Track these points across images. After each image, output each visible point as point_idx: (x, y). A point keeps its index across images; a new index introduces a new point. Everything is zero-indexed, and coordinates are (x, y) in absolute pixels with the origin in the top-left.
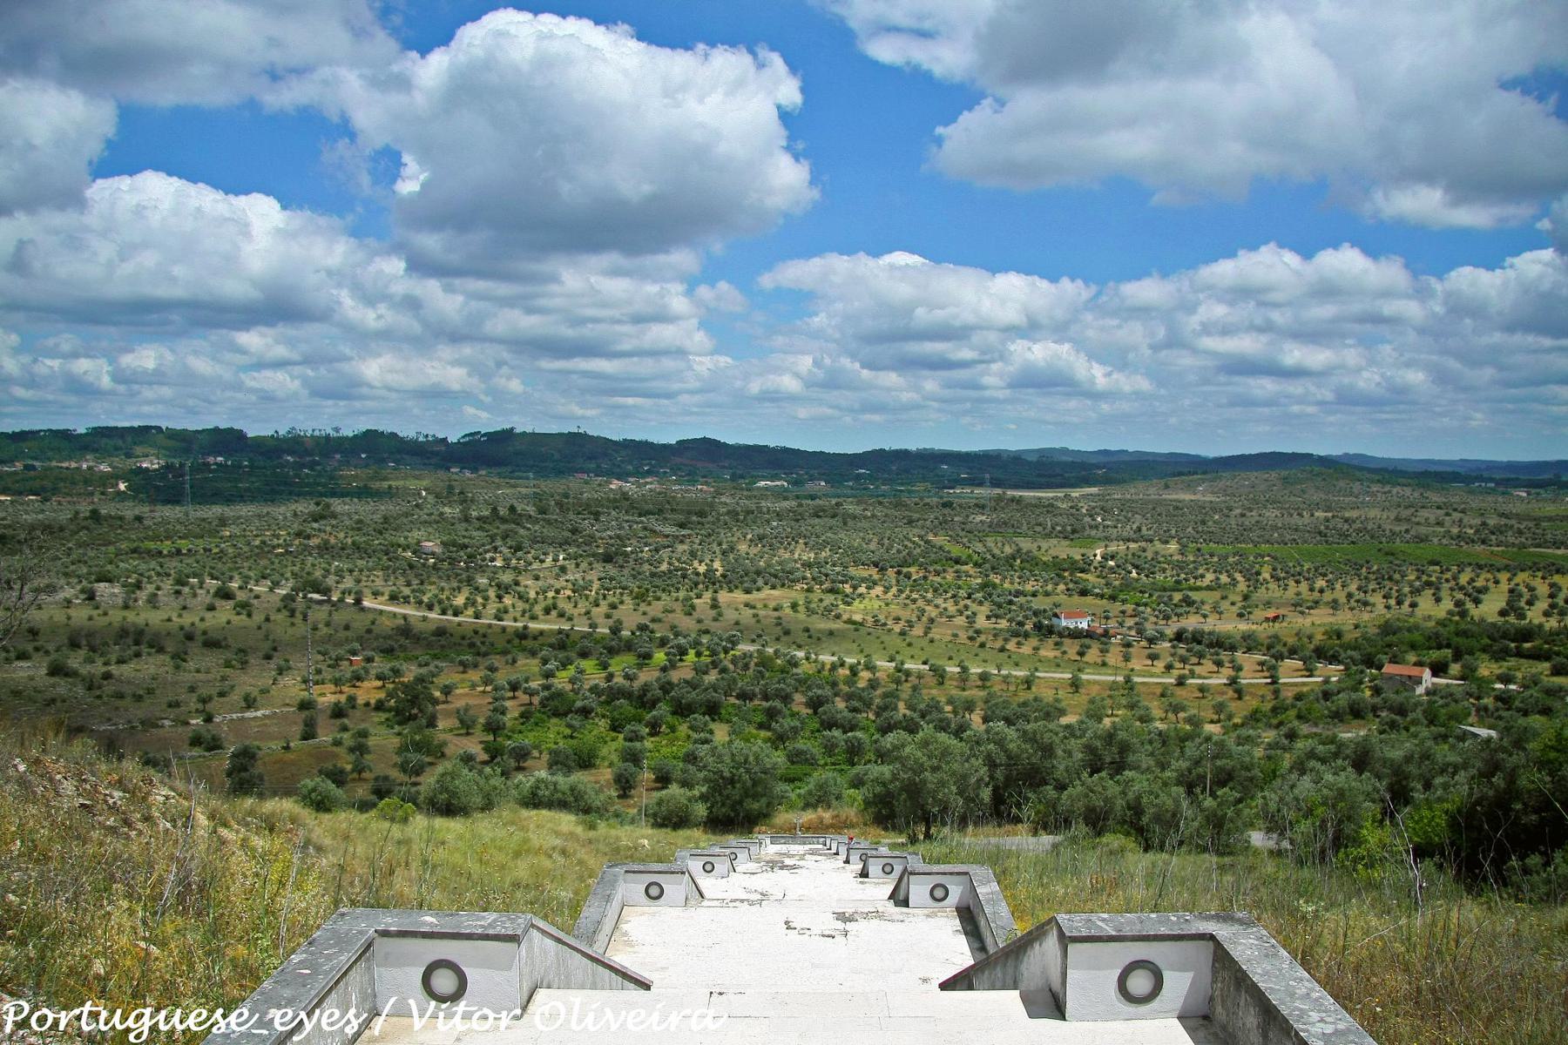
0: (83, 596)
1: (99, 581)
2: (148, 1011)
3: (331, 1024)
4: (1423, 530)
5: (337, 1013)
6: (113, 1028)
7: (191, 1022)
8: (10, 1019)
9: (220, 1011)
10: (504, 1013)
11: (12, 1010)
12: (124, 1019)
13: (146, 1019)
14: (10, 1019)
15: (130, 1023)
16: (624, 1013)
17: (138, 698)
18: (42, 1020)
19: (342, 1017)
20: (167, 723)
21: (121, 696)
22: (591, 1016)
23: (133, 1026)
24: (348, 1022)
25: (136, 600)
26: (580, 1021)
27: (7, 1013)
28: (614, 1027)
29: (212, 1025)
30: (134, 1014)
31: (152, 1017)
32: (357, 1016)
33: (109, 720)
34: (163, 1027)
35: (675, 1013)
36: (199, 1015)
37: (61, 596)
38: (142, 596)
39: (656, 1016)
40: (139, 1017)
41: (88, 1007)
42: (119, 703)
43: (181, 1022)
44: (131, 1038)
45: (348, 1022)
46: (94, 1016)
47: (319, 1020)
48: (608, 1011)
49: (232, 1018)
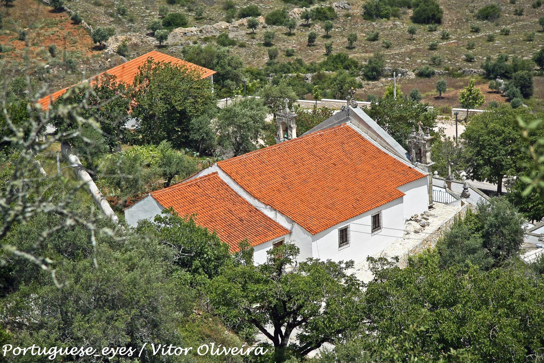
2: (56, 348)
5: (77, 349)
6: (216, 354)
11: (6, 348)
15: (49, 352)
18: (17, 351)
19: (78, 350)
23: (50, 353)
24: (81, 352)
26: (214, 351)
28: (226, 354)
30: (50, 349)
31: (57, 350)
34: (61, 354)
36: (235, 349)
38: (22, 61)
40: (53, 350)
41: (34, 347)
43: (68, 352)
44: (50, 358)
45: (81, 352)
47: (230, 351)
48: (224, 348)
49: (87, 351)
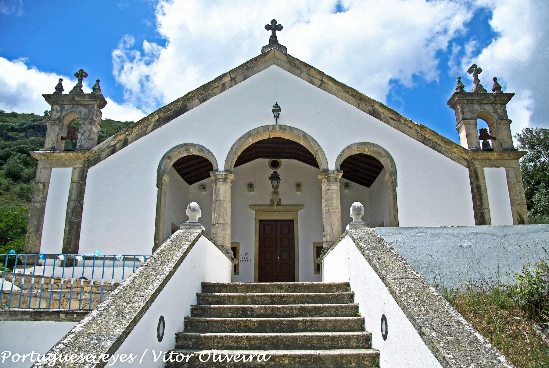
10: (24, 355)
11: (5, 354)
14: (4, 358)
18: (16, 358)
24: (80, 359)
32: (133, 357)
41: (33, 353)
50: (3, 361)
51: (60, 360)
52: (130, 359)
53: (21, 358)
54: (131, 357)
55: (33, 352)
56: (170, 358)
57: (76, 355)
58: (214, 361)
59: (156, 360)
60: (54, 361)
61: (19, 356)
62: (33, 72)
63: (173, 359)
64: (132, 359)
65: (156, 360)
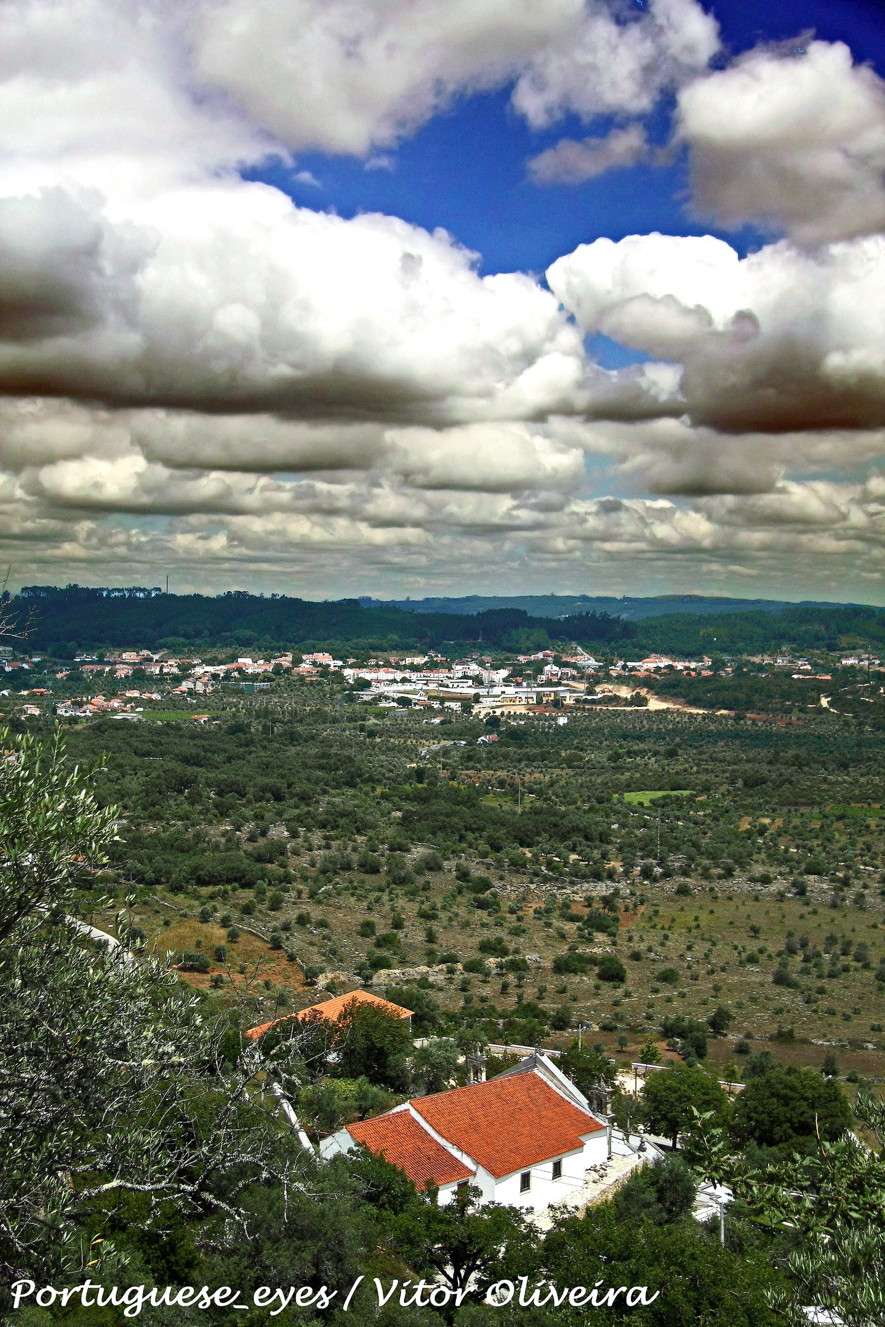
0: (794, 890)
1: (809, 872)
3: (579, 1300)
4: (351, 725)
7: (179, 1298)
8: (18, 1296)
9: (206, 1289)
10: (66, 1291)
11: (20, 1288)
12: (119, 1296)
13: (139, 1296)
14: (18, 1296)
15: (125, 1299)
16: (566, 1290)
17: (847, 1018)
18: (46, 1296)
20: (870, 1046)
21: (832, 1012)
22: (537, 1293)
23: (127, 1302)
24: (320, 1298)
25: (843, 900)
27: (15, 1291)
28: (557, 1303)
29: (198, 1302)
32: (328, 1293)
33: (825, 1035)
35: (612, 1290)
37: (773, 888)
39: (595, 1293)
41: (87, 1285)
42: (831, 1020)
46: (92, 1294)
49: (217, 1296)
50: (16, 1306)
51: (154, 1303)
52: (202, 1298)
53: (59, 1298)
54: (205, 1296)
55: (88, 1282)
56: (417, 1296)
57: (310, 1290)
58: (523, 1303)
59: (382, 1301)
60: (139, 1305)
61: (54, 1293)
62: (548, 594)
63: (423, 1300)
64: (326, 1300)
65: (382, 1301)
